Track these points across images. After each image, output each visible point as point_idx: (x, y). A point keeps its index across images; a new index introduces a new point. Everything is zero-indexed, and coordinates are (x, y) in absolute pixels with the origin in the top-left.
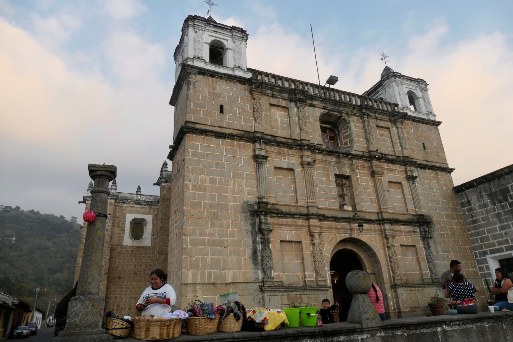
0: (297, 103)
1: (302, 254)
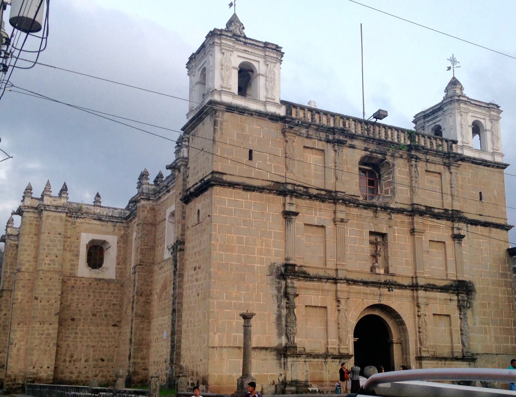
0: (335, 145)
1: (327, 320)
